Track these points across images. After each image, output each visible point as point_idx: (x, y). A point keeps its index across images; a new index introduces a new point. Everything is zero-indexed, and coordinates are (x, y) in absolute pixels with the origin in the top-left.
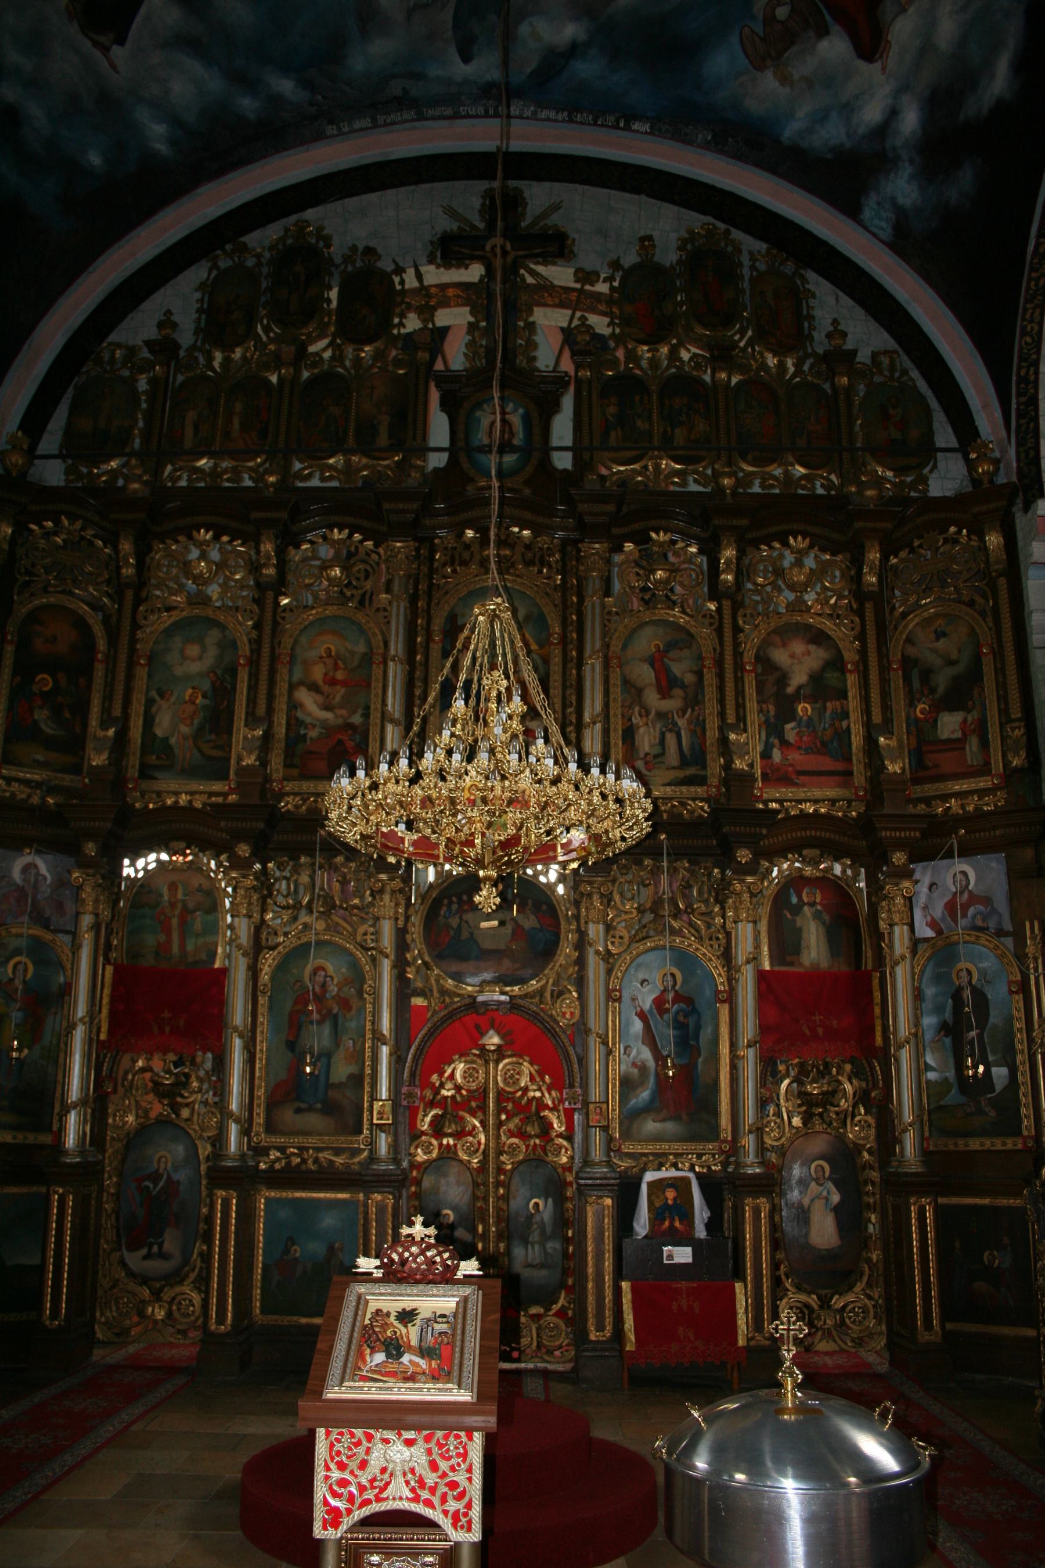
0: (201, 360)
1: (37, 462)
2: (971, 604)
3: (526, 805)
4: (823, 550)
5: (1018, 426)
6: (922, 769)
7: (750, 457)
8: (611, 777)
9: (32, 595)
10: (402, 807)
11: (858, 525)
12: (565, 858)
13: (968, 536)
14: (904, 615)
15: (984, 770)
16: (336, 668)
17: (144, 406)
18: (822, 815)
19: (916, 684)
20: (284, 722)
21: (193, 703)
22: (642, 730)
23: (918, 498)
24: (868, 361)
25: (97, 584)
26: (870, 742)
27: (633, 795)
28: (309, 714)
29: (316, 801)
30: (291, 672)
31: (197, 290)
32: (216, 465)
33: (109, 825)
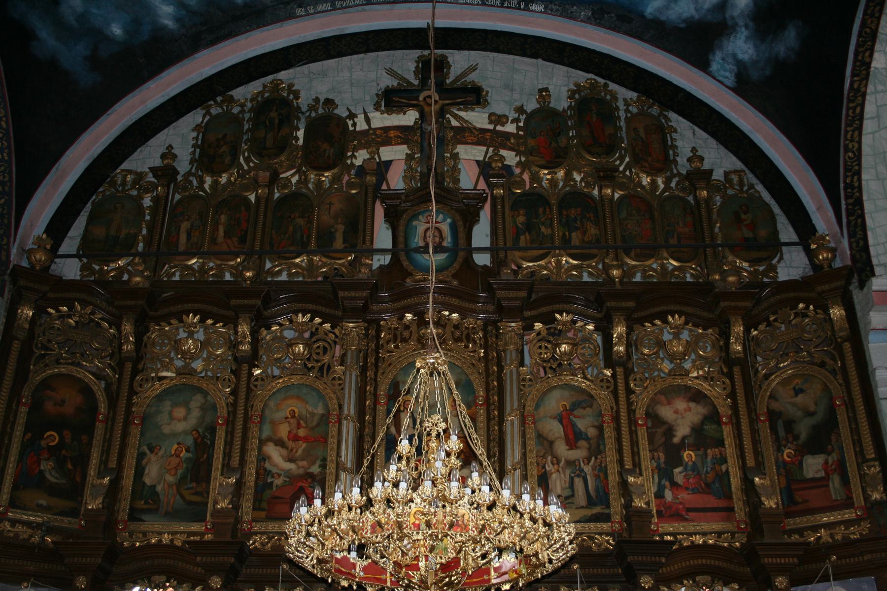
0: (195, 183)
1: (56, 260)
2: (822, 365)
3: (465, 528)
4: (696, 325)
5: (849, 223)
6: (793, 504)
7: (633, 254)
8: (540, 503)
9: (46, 365)
10: (354, 531)
11: (723, 304)
12: (498, 580)
13: (815, 310)
14: (766, 377)
15: (848, 503)
16: (299, 426)
17: (148, 218)
18: (710, 545)
19: (782, 433)
20: (254, 472)
21: (178, 456)
22: (554, 476)
23: (769, 283)
24: (722, 179)
25: (102, 358)
26: (747, 482)
27: (559, 520)
28: (276, 466)
29: (279, 540)
30: (260, 430)
31: (193, 130)
32: (203, 264)
33: (99, 561)
